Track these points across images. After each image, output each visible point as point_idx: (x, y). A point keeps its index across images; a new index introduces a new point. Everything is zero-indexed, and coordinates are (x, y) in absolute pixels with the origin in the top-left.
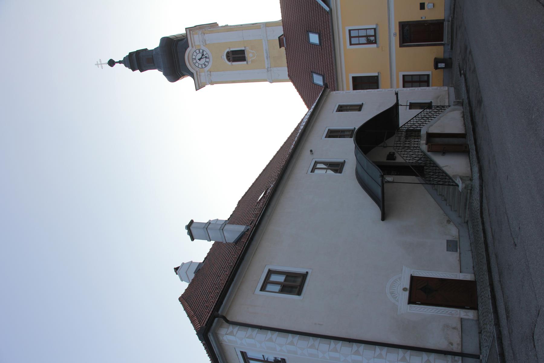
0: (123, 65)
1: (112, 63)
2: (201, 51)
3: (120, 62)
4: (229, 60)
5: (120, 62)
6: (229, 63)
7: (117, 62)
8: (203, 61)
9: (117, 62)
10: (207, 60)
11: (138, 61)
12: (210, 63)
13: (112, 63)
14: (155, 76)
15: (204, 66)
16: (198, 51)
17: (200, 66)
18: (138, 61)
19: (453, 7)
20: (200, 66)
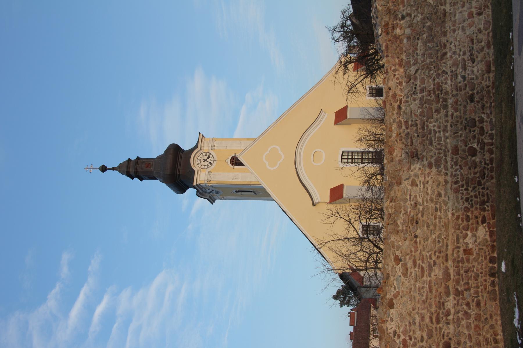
0: (116, 172)
1: (104, 169)
2: (208, 154)
3: (113, 169)
4: (232, 164)
5: (113, 169)
6: (232, 166)
7: (110, 169)
8: (206, 163)
9: (110, 169)
10: (209, 165)
11: (136, 169)
12: (213, 166)
13: (104, 169)
14: (157, 188)
15: (206, 167)
16: (204, 154)
17: (203, 167)
18: (136, 169)
19: (240, 193)
20: (203, 167)
